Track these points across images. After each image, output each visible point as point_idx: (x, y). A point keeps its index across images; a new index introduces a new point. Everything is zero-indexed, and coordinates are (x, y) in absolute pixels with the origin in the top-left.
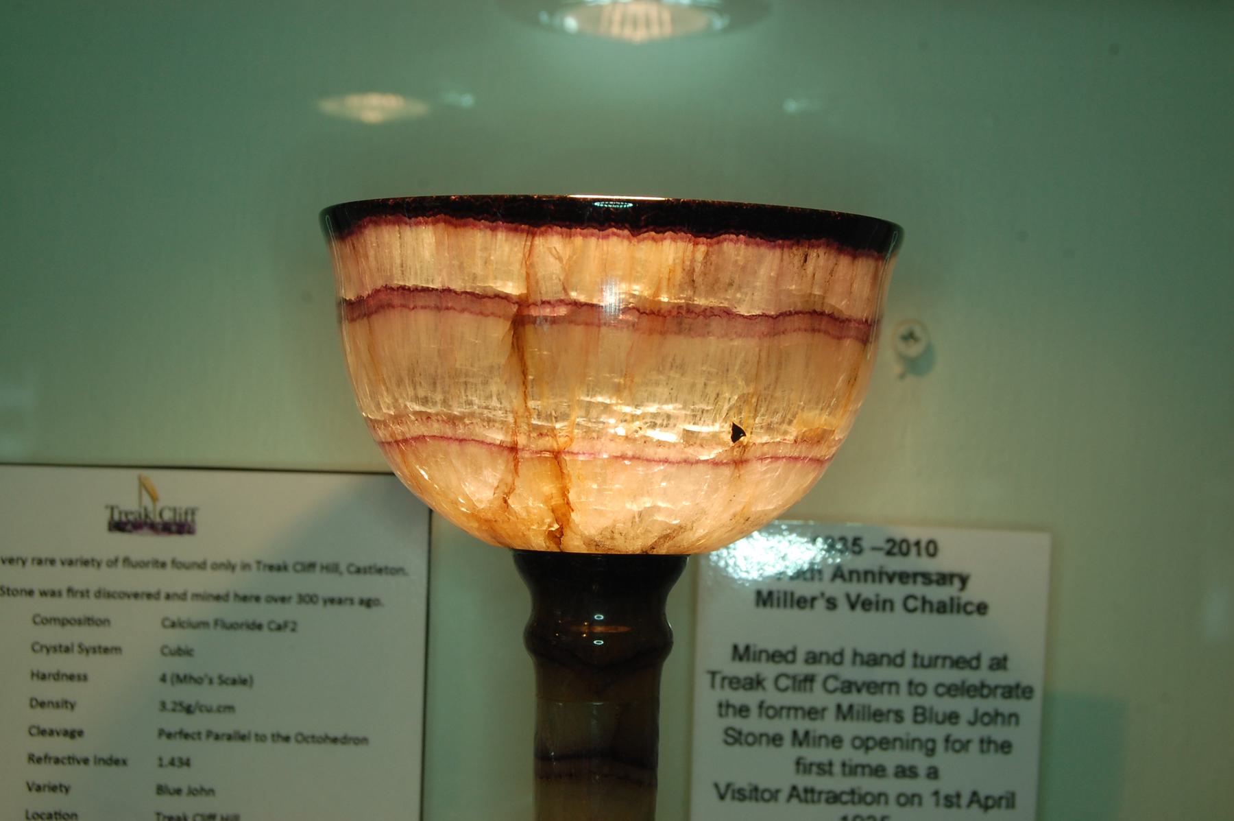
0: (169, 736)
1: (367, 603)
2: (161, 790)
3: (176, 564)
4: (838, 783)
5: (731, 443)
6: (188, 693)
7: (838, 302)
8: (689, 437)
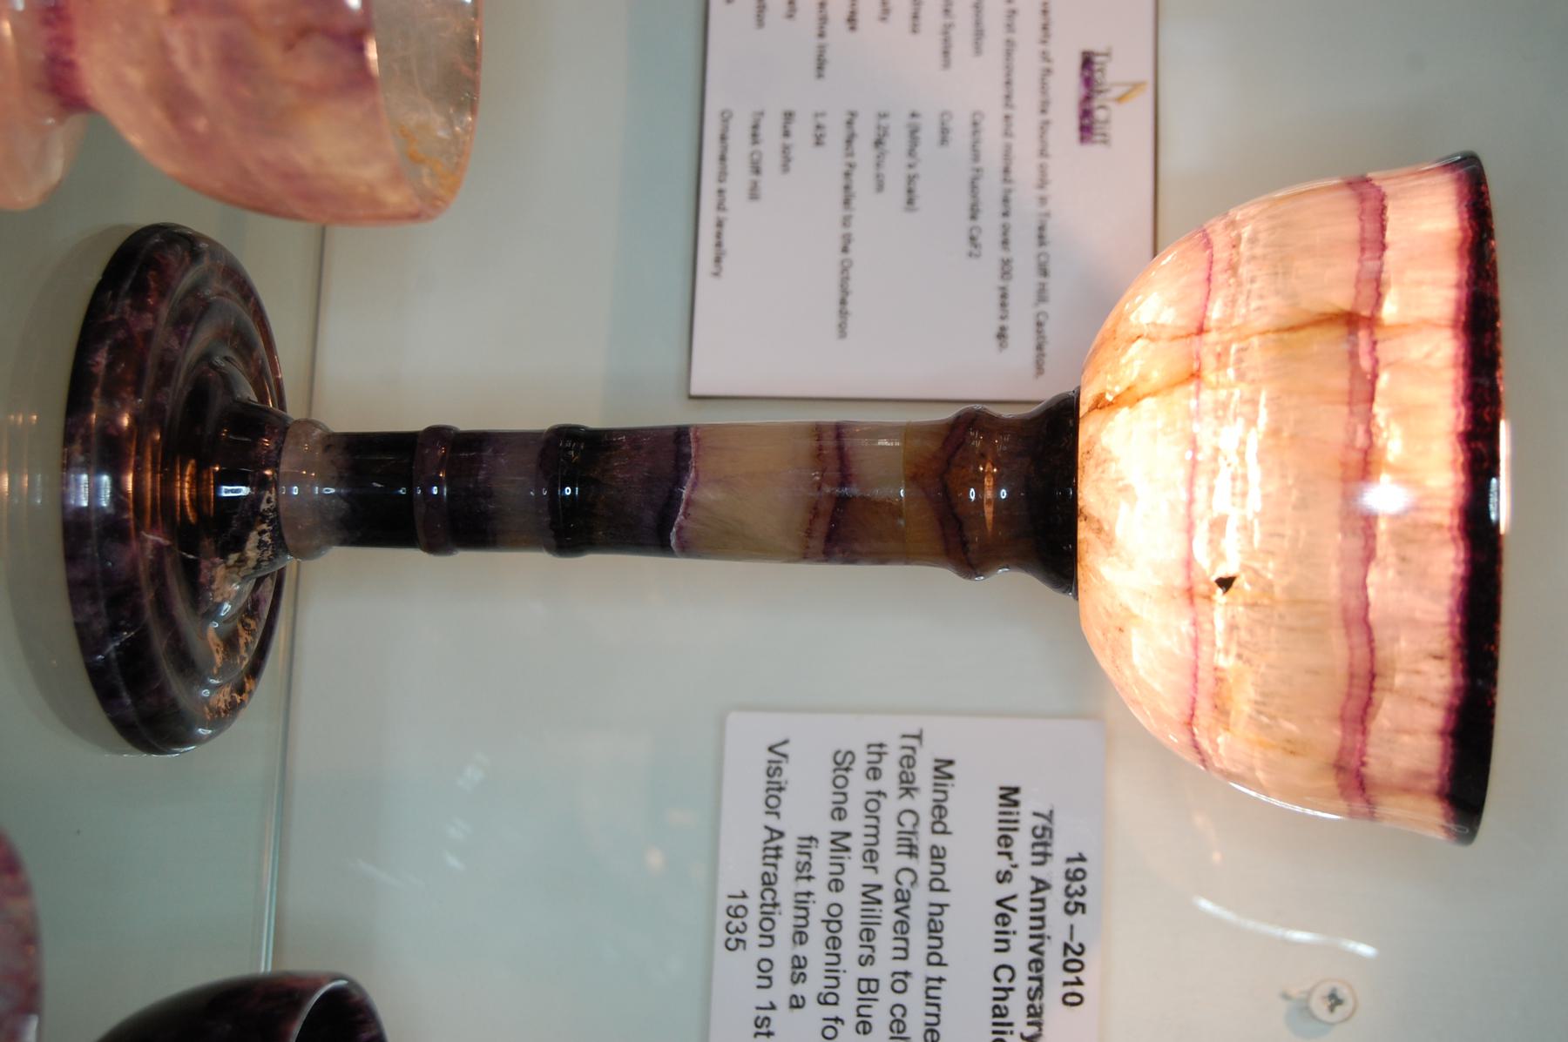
0: (850, 123)
1: (1002, 335)
2: (789, 116)
3: (1044, 126)
4: (786, 888)
5: (1214, 578)
6: (897, 143)
7: (1387, 713)
8: (1218, 525)
